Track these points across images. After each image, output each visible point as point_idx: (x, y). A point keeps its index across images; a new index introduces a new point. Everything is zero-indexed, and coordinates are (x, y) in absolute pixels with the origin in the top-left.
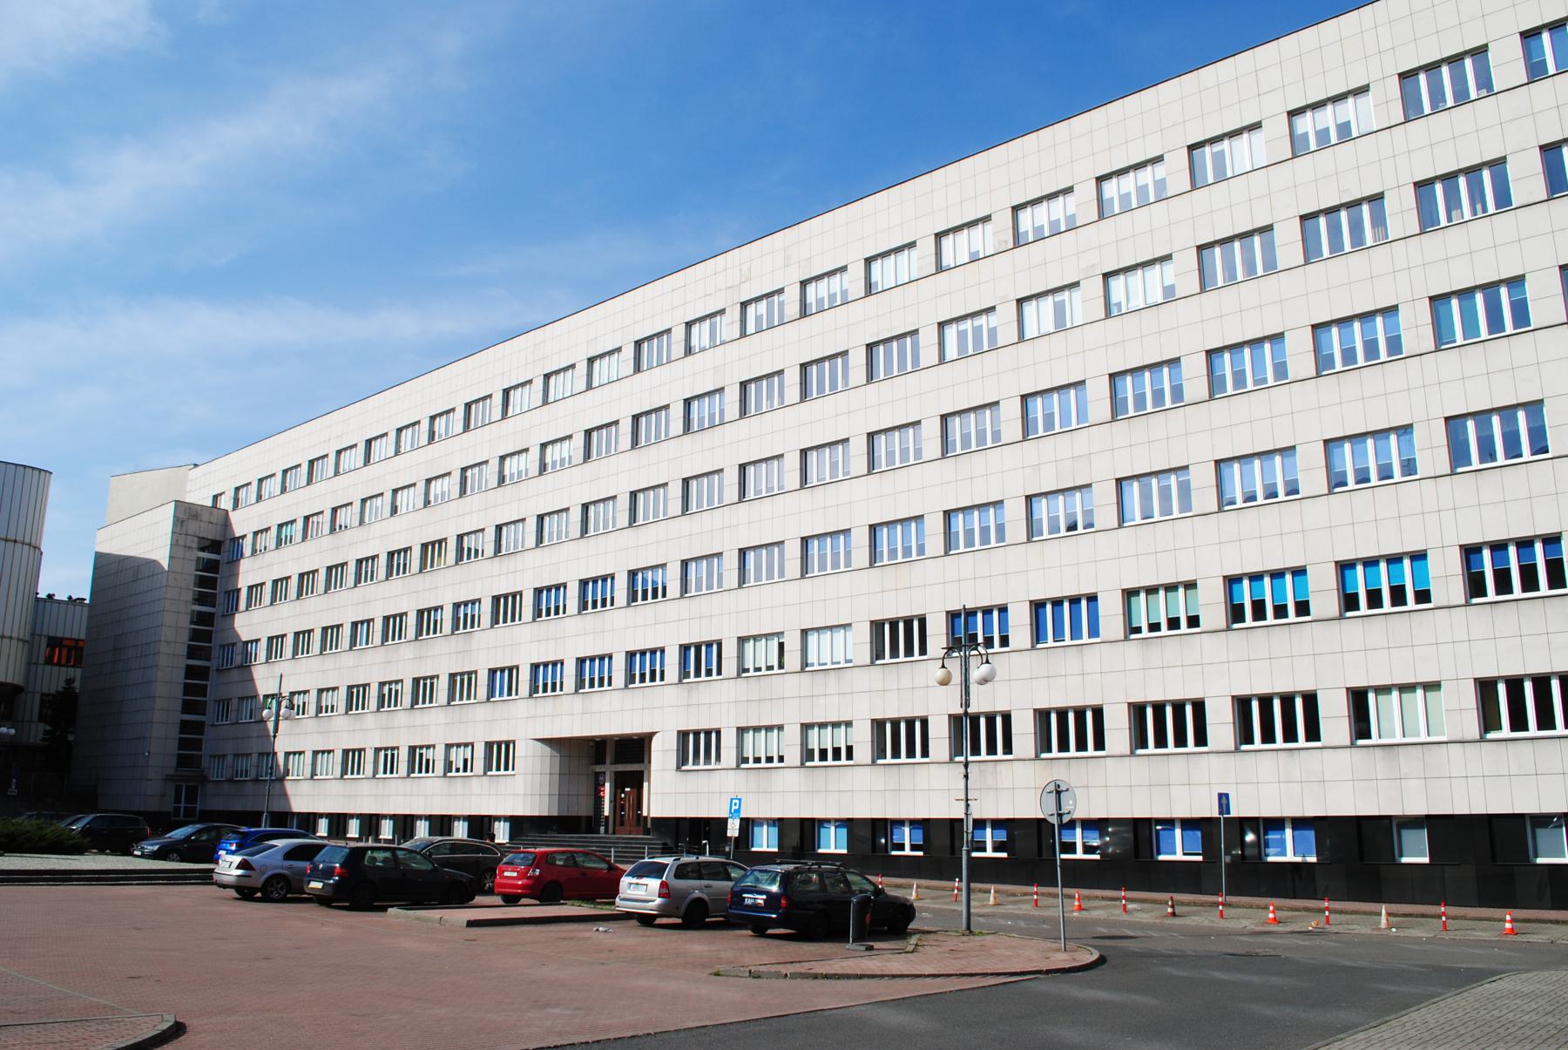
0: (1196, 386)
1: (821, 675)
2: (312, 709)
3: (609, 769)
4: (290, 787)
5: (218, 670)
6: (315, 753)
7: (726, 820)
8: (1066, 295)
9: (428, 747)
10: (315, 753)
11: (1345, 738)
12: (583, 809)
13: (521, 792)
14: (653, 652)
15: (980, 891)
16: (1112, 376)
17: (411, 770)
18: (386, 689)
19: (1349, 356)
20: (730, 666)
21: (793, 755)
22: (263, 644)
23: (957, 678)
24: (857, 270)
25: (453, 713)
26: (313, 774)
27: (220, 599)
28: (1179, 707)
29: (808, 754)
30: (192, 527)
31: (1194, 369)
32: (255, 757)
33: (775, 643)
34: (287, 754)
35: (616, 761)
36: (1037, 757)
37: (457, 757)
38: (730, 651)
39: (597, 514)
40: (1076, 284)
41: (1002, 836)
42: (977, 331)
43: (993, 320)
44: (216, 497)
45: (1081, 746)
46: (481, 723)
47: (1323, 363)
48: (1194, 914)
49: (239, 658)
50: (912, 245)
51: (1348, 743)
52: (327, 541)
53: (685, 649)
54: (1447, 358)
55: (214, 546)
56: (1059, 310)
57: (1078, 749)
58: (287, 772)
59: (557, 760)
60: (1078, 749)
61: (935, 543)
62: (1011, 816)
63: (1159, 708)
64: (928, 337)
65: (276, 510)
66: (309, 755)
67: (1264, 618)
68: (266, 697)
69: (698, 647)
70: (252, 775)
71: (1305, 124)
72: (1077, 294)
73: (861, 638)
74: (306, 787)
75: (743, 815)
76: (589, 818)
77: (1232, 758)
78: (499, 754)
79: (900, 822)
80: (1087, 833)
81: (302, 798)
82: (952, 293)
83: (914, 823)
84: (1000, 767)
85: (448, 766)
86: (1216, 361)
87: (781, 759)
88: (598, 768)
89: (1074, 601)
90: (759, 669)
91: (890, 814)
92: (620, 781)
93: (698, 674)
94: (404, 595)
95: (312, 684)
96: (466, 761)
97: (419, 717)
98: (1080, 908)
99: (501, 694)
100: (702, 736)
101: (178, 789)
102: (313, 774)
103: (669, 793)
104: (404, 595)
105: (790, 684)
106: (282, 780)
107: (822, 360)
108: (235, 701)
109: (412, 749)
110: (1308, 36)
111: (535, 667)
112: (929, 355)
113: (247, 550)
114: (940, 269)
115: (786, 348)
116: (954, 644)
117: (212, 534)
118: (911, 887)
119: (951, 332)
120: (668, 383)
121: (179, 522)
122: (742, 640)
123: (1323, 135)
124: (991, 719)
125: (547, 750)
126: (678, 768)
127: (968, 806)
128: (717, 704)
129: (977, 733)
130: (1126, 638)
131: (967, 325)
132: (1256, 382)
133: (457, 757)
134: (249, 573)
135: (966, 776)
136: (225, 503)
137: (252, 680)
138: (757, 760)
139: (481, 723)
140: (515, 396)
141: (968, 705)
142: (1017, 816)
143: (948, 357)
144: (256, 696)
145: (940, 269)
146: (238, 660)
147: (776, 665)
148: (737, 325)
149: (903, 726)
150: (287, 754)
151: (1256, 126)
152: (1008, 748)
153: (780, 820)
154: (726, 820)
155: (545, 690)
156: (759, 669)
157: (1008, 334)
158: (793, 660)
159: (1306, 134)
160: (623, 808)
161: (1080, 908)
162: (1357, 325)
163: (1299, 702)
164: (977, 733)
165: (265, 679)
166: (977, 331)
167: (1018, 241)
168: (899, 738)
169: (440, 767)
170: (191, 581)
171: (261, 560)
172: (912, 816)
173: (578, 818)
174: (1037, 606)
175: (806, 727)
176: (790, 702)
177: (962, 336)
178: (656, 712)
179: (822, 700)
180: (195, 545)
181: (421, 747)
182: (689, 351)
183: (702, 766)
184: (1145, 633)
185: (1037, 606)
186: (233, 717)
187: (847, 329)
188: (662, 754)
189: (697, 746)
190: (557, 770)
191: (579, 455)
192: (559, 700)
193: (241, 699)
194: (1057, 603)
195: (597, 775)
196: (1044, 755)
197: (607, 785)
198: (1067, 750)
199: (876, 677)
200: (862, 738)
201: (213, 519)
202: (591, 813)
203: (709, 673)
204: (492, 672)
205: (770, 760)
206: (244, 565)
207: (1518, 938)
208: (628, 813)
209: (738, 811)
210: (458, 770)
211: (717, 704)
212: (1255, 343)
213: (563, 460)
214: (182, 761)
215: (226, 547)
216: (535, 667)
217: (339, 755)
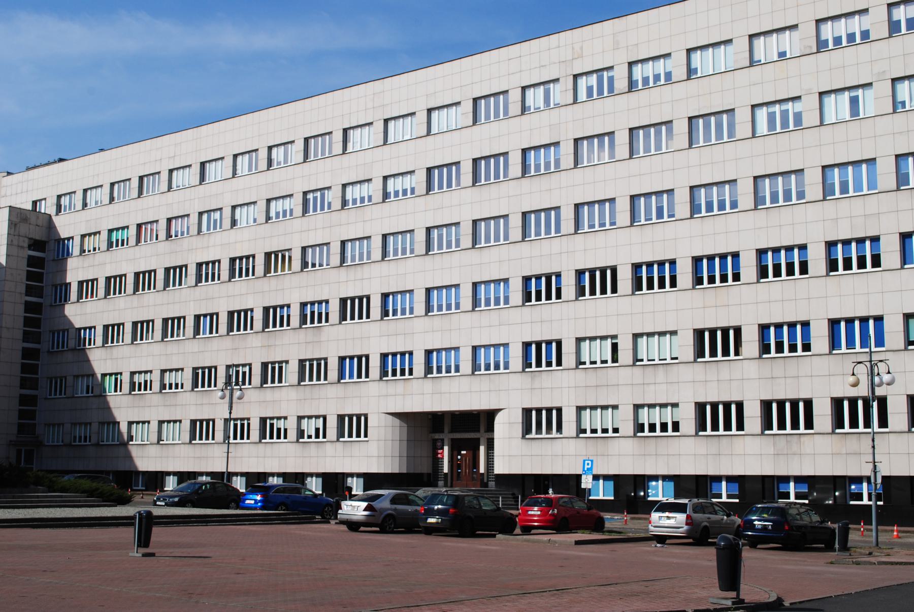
0: (814, 190)
1: (650, 369)
2: (156, 386)
3: (447, 436)
4: (134, 451)
5: (49, 352)
6: (161, 423)
7: (579, 477)
8: (860, 92)
9: (279, 418)
10: (161, 423)
11: (829, 429)
12: (424, 468)
13: (377, 453)
14: (403, 354)
15: (855, 529)
16: (755, 178)
17: (263, 436)
18: (233, 372)
19: (774, 198)
20: (569, 359)
21: (627, 428)
22: (100, 331)
23: (227, 398)
24: (680, 58)
25: (301, 392)
26: (160, 439)
27: (48, 291)
28: (794, 404)
29: (640, 428)
30: (23, 229)
31: (813, 178)
32: (95, 427)
33: (609, 342)
34: (130, 423)
35: (452, 431)
36: (762, 434)
37: (309, 427)
38: (568, 349)
39: (440, 237)
40: (870, 85)
41: (804, 489)
42: (785, 114)
43: (798, 106)
44: (35, 203)
45: (728, 427)
46: (333, 400)
47: (758, 200)
48: (907, 537)
49: (74, 342)
50: (728, 42)
51: (830, 431)
52: (164, 246)
53: (527, 345)
54: (760, 215)
55: (36, 245)
56: (854, 101)
57: (779, 429)
58: (131, 438)
59: (405, 429)
60: (779, 429)
61: (420, 308)
62: (813, 474)
63: (781, 404)
64: (743, 116)
65: (103, 217)
66: (154, 425)
67: (729, 355)
68: (104, 375)
69: (539, 345)
70: (94, 440)
71: (828, 32)
72: (869, 93)
73: (686, 341)
74: (154, 450)
75: (595, 472)
76: (429, 475)
77: (758, 439)
78: (353, 425)
79: (718, 479)
80: (731, 485)
81: (146, 459)
82: (768, 83)
83: (730, 479)
84: (803, 439)
85: (301, 434)
86: (902, 163)
87: (616, 430)
88: (437, 436)
89: (864, 320)
90: (595, 363)
91: (711, 472)
92: (455, 448)
93: (539, 364)
94: (223, 297)
95: (156, 365)
96: (317, 430)
97: (268, 394)
98: (898, 537)
99: (351, 376)
100: (544, 412)
101: (19, 452)
102: (160, 439)
103: (512, 453)
104: (223, 297)
105: (623, 375)
106: (125, 445)
107: (539, 147)
108: (70, 379)
109: (263, 421)
110: (608, 27)
111: (384, 356)
112: (743, 129)
113: (76, 251)
114: (752, 63)
115: (618, 113)
116: (228, 382)
117: (38, 235)
118: (893, 531)
119: (762, 115)
120: (506, 135)
121: (12, 225)
122: (579, 340)
123: (837, 41)
124: (727, 406)
125: (397, 422)
126: (523, 437)
127: (875, 467)
128: (558, 388)
129: (238, 429)
130: (906, 349)
131: (777, 108)
132: (669, 216)
133: (309, 427)
134: (76, 270)
135: (873, 447)
136: (48, 208)
137: (88, 361)
138: (594, 431)
139: (333, 400)
140: (354, 135)
141: (230, 413)
142: (817, 474)
143: (759, 132)
144: (93, 375)
145: (752, 63)
146: (72, 344)
147: (609, 359)
148: (382, 135)
149: (721, 408)
150: (130, 423)
151: (794, 27)
152: (740, 427)
153: (247, 473)
154: (579, 477)
155: (394, 374)
156: (595, 363)
157: (811, 118)
158: (625, 355)
159: (899, 21)
160: (459, 466)
161: (898, 537)
162: (864, 166)
163: (801, 405)
164: (238, 429)
165: (101, 360)
166: (785, 114)
167: (821, 45)
168: (718, 416)
169: (292, 435)
170: (24, 276)
171: (88, 260)
172: (605, 473)
173: (421, 475)
174: (834, 324)
175: (637, 407)
176: (624, 387)
177: (771, 118)
178: (507, 394)
179: (652, 387)
180: (26, 245)
181: (272, 418)
182: (524, 109)
183: (544, 435)
184: (588, 365)
185: (834, 324)
186: (69, 392)
187: (676, 103)
188: (506, 429)
189: (539, 421)
190: (390, 437)
191: (422, 188)
192: (409, 383)
193: (76, 377)
194: (850, 321)
195: (435, 441)
196: (639, 434)
197: (446, 448)
198: (541, 433)
199: (698, 370)
200: (687, 417)
201: (40, 223)
202: (430, 471)
203: (549, 364)
204: (342, 359)
205: (605, 431)
206: (72, 263)
207: (899, 540)
208: (465, 470)
209: (590, 469)
210: (310, 437)
211: (558, 388)
212: (856, 163)
213: (285, 212)
214: (21, 429)
215: (52, 246)
216: (384, 356)
217: (186, 425)
